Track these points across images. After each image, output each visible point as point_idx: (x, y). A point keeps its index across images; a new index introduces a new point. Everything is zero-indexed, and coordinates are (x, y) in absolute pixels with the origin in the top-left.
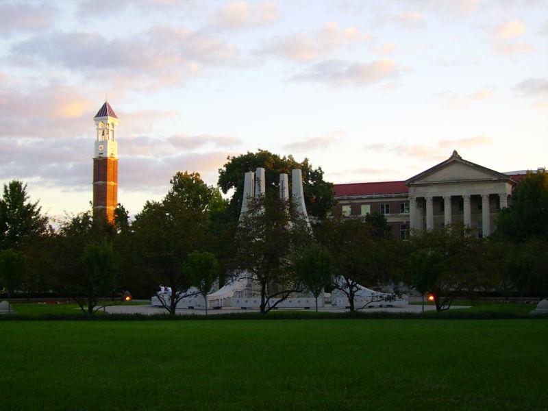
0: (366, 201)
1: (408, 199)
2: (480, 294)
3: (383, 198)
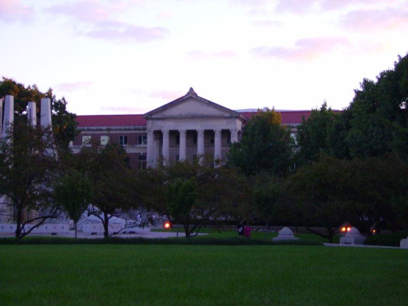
0: (105, 132)
1: (146, 131)
2: (226, 222)
3: (131, 130)
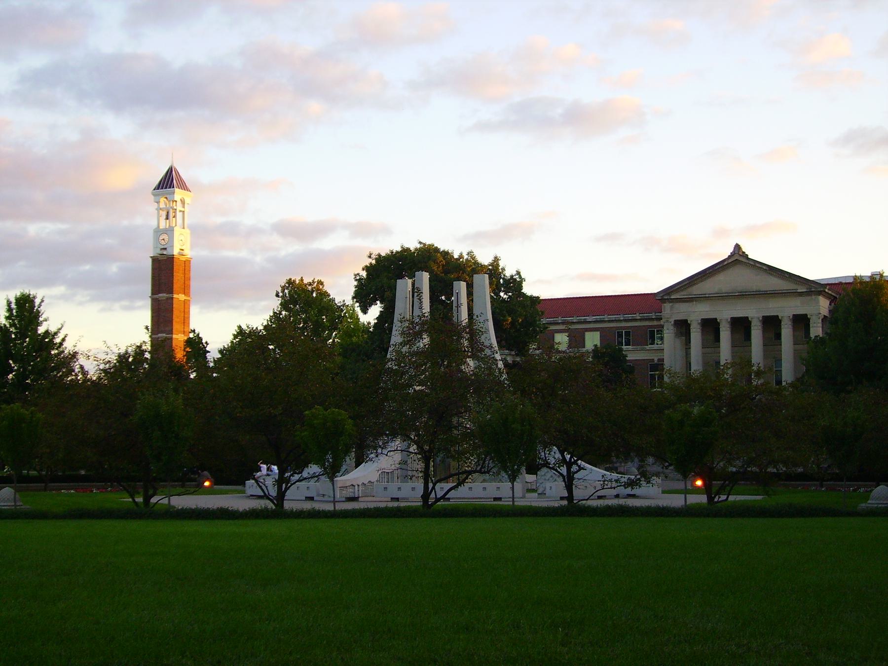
1: (662, 322)
2: (777, 476)
